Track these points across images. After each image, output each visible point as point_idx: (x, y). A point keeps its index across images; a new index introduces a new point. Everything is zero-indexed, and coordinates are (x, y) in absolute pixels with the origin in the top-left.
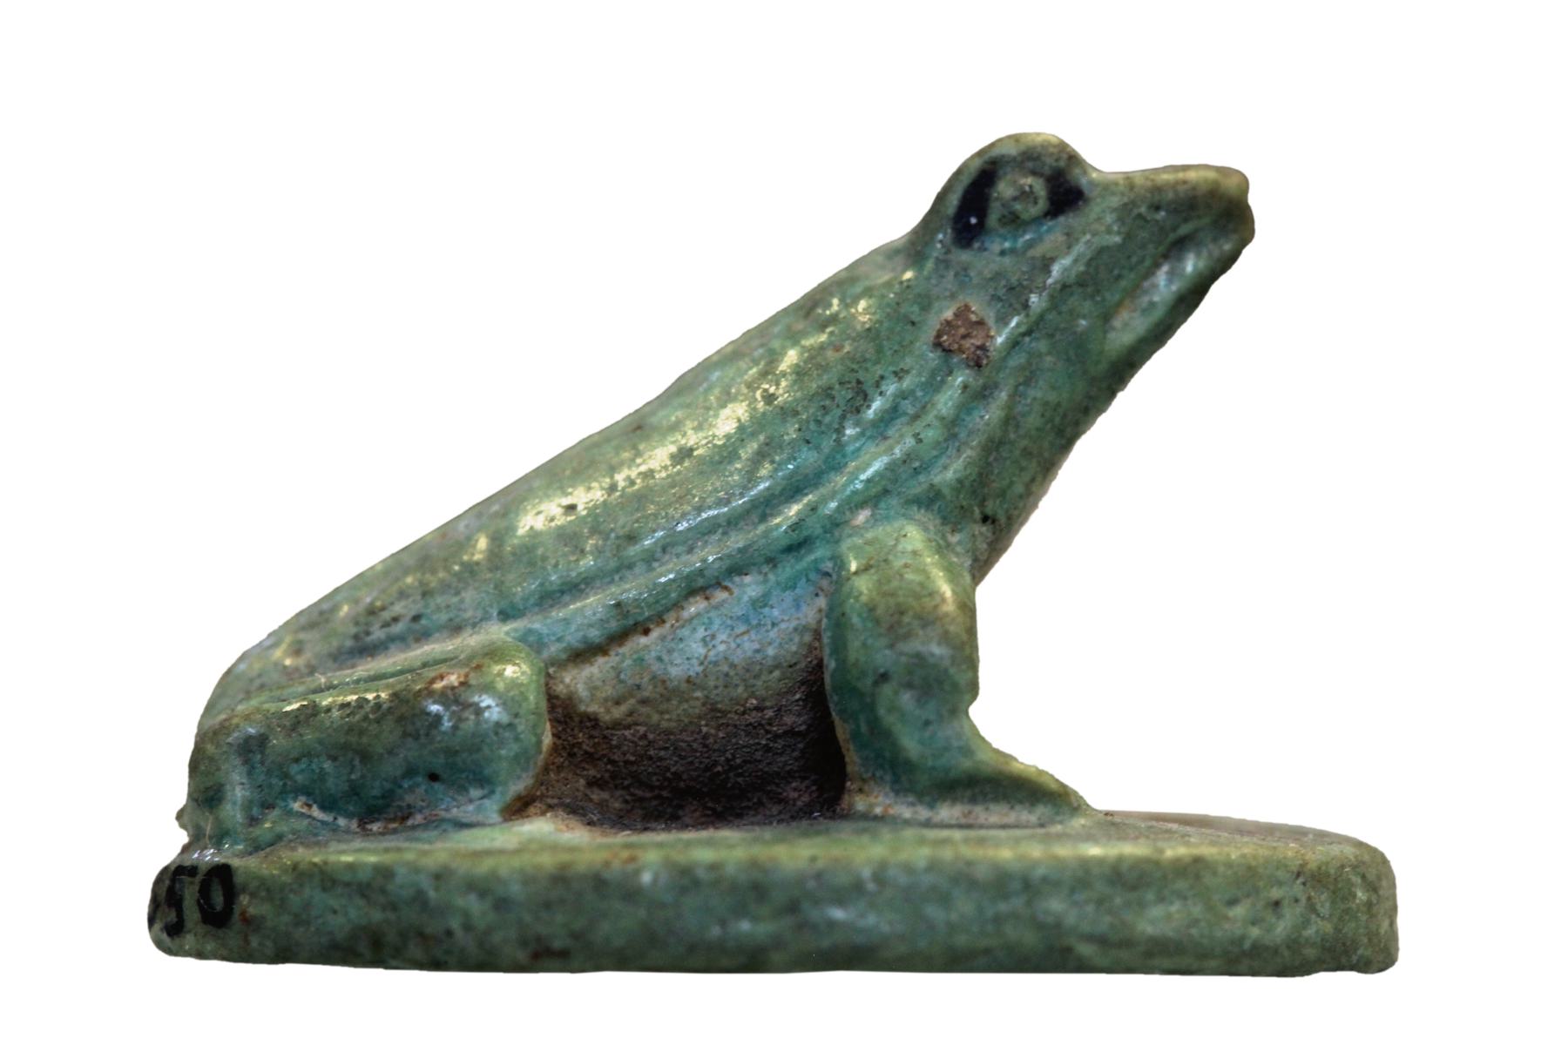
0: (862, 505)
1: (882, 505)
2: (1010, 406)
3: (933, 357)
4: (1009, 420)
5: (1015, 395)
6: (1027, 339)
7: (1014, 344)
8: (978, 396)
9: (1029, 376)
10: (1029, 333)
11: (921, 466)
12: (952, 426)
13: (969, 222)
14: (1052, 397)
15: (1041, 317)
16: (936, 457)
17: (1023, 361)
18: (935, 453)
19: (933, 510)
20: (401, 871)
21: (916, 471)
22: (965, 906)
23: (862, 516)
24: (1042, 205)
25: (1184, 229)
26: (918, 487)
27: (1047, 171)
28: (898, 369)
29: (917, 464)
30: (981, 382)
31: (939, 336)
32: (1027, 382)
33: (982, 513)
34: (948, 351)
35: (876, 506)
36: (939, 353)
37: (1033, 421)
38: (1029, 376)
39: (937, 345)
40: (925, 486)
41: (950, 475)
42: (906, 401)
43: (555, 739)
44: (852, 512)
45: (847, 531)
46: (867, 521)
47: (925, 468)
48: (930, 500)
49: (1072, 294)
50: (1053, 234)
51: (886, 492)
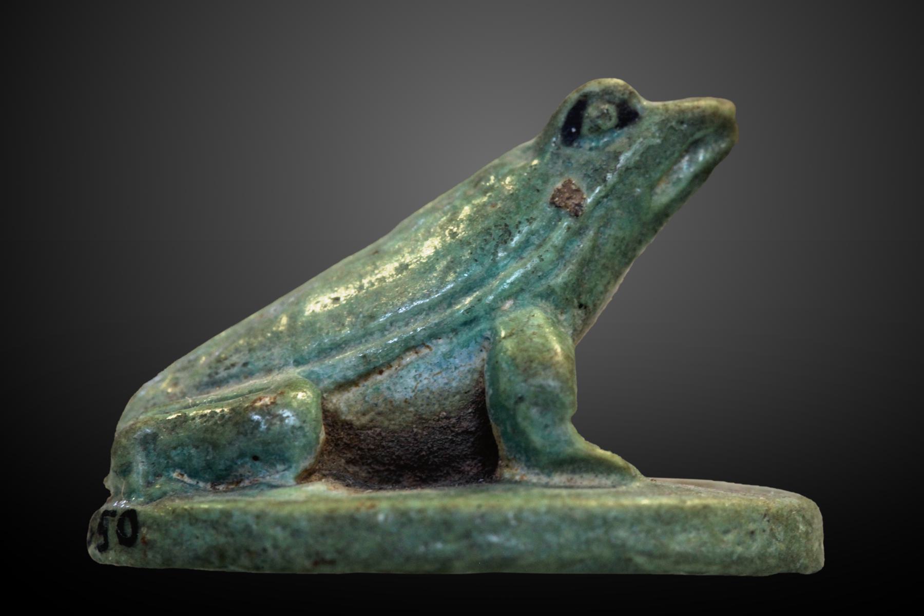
0: (508, 298)
1: (520, 298)
2: (595, 239)
3: (550, 211)
4: (595, 248)
5: (598, 233)
6: (605, 200)
7: (598, 203)
8: (576, 233)
9: (606, 222)
10: (606, 196)
11: (543, 275)
12: (561, 251)
13: (571, 131)
14: (620, 234)
15: (614, 187)
16: (551, 269)
17: (603, 213)
18: (551, 267)
19: (550, 301)
20: (236, 514)
21: (540, 278)
22: (568, 534)
23: (508, 304)
24: (614, 121)
25: (698, 135)
26: (541, 287)
27: (617, 101)
28: (529, 218)
29: (540, 274)
30: (578, 225)
31: (553, 198)
32: (605, 225)
33: (579, 302)
34: (558, 207)
35: (516, 298)
36: (553, 208)
37: (609, 248)
39: (552, 203)
40: (545, 287)
41: (560, 280)
43: (327, 436)
44: (502, 302)
45: (499, 313)
46: (511, 307)
47: (545, 276)
48: (548, 295)
49: (632, 173)
50: (620, 138)
51: (522, 290)
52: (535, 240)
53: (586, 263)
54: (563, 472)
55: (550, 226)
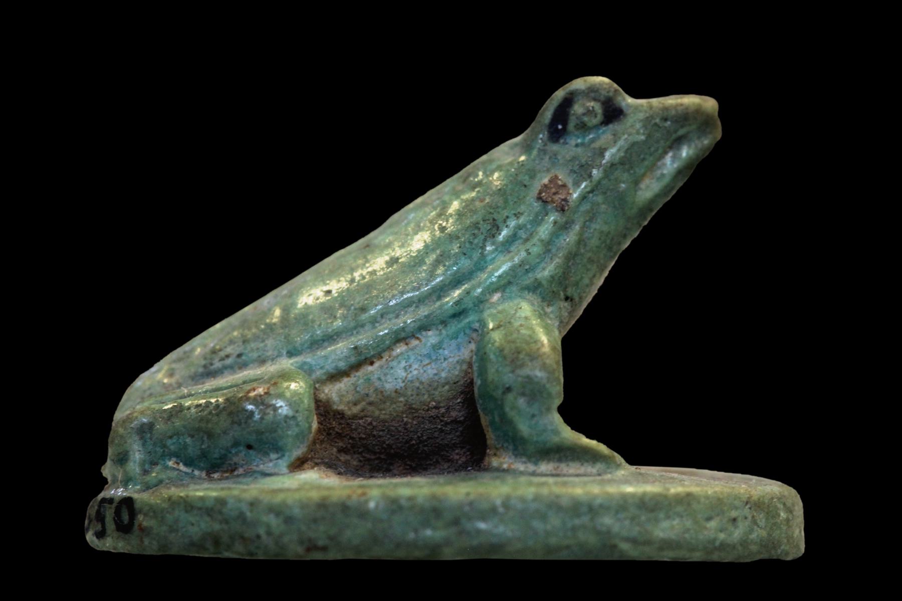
0: (496, 290)
1: (508, 290)
2: (581, 234)
3: (537, 205)
4: (581, 242)
5: (584, 227)
6: (591, 195)
7: (583, 198)
8: (563, 228)
9: (592, 216)
10: (592, 191)
11: (530, 268)
12: (548, 245)
13: (557, 127)
14: (605, 228)
15: (599, 182)
16: (538, 263)
17: (588, 207)
18: (538, 260)
19: (536, 293)
20: (231, 501)
21: (527, 271)
22: (555, 521)
23: (496, 297)
24: (600, 118)
25: (681, 132)
26: (528, 280)
27: (602, 98)
28: (516, 212)
29: (527, 267)
30: (564, 219)
31: (540, 193)
32: (591, 220)
33: (565, 295)
34: (545, 202)
35: (504, 291)
36: (540, 203)
37: (594, 242)
38: (592, 216)
39: (539, 198)
40: (532, 280)
41: (546, 273)
42: (521, 231)
43: (320, 425)
44: (490, 295)
45: (487, 305)
46: (499, 300)
47: (532, 269)
48: (535, 287)
51: (510, 283)
52: (522, 234)
53: (572, 257)
54: (549, 460)
55: (537, 221)
